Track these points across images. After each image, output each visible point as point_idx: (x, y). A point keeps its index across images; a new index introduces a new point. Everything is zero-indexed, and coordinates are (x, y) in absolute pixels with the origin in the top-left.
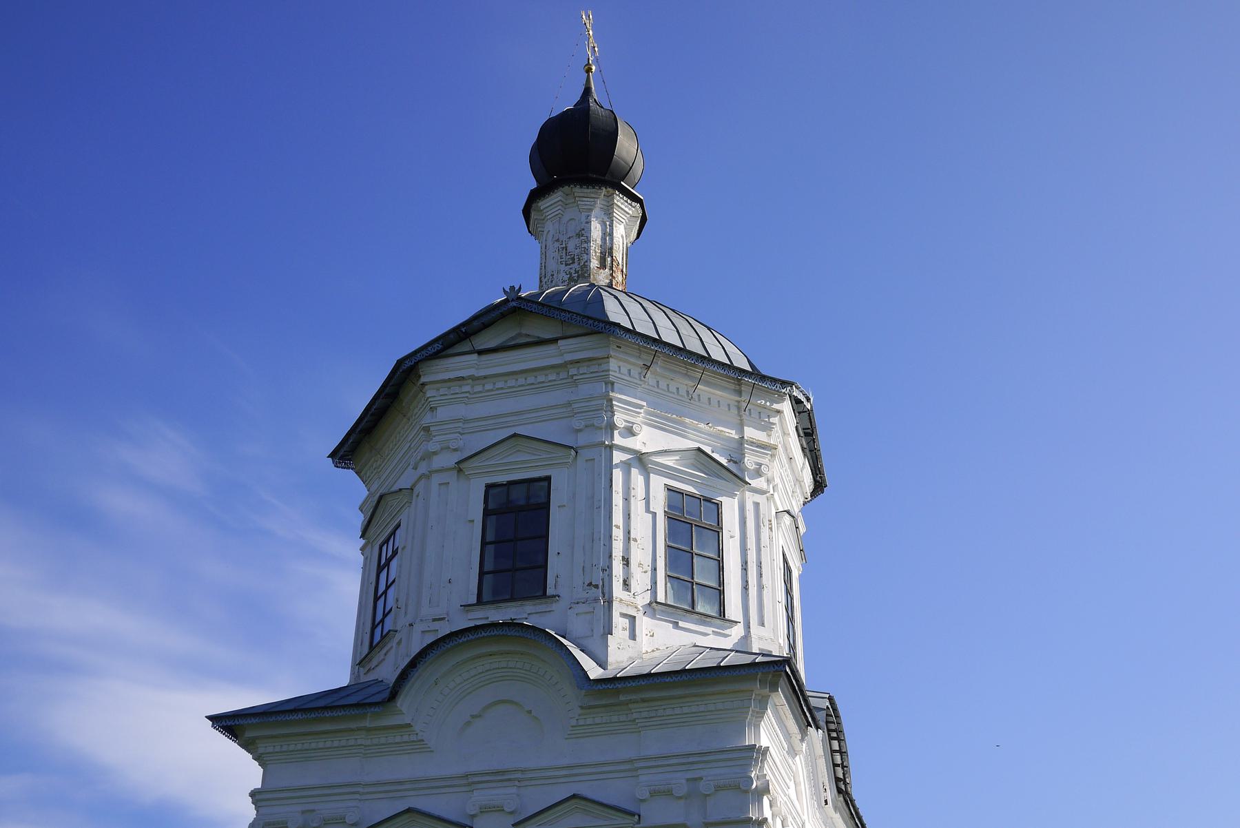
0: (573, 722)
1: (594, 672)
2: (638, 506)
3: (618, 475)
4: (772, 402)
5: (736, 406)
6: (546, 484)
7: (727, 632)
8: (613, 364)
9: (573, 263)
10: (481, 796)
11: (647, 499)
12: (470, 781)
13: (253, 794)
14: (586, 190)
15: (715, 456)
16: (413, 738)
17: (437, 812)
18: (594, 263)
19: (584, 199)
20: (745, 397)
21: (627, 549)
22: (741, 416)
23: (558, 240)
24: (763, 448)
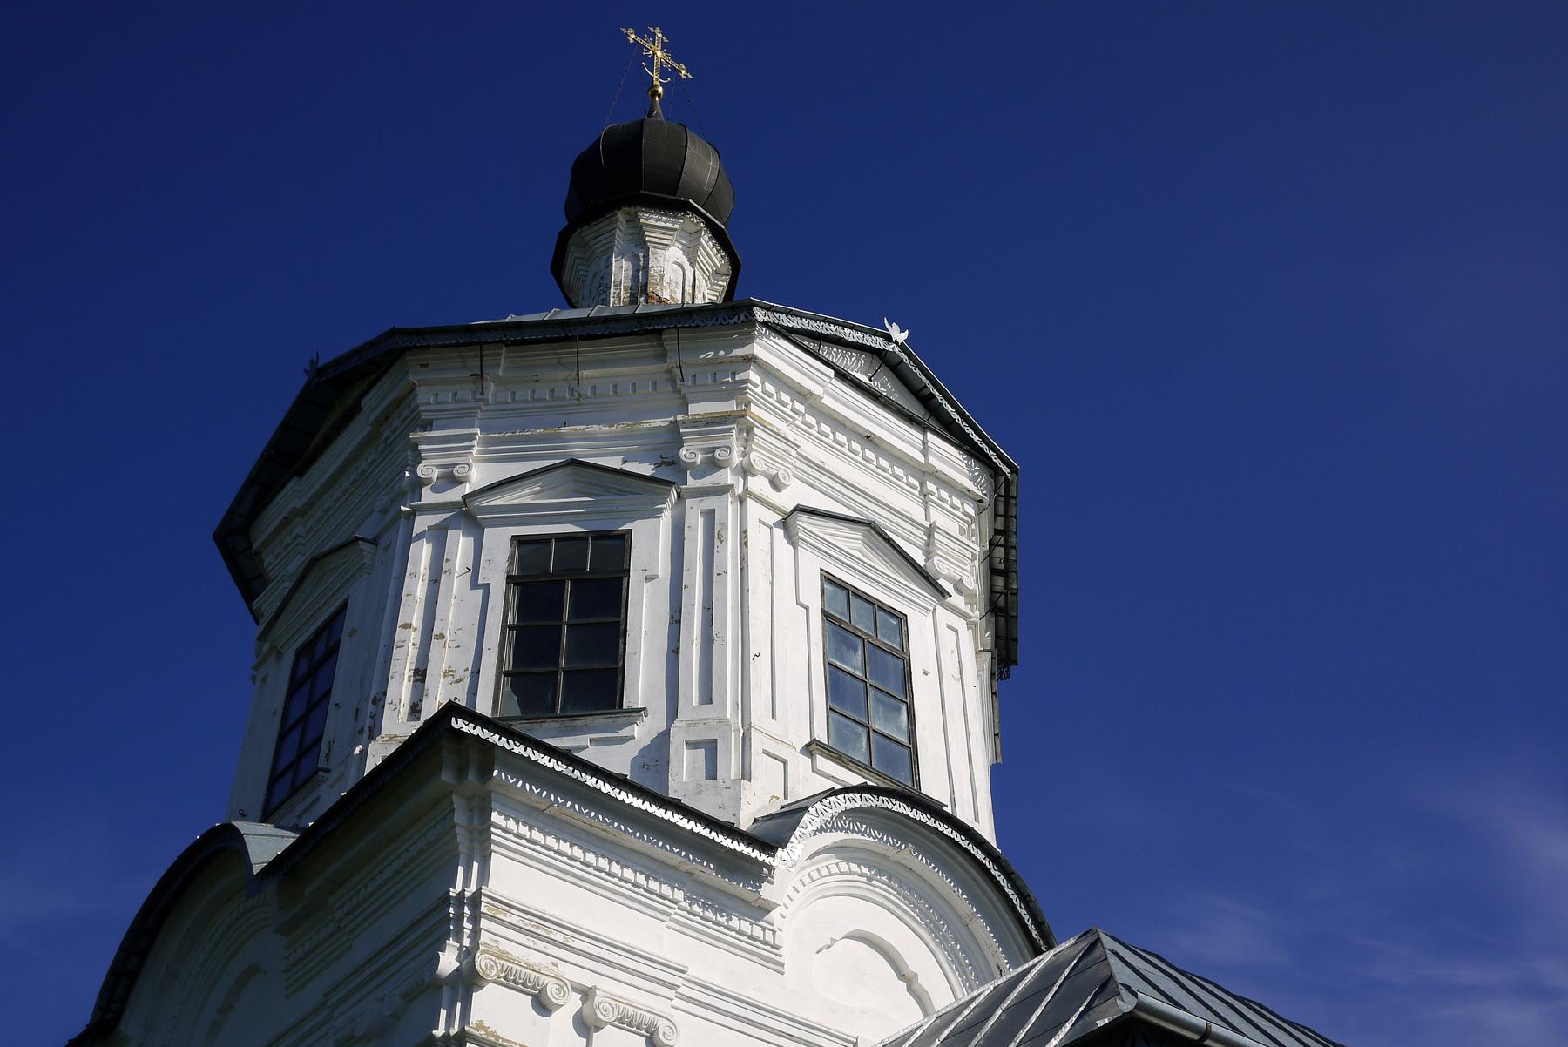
4: (729, 349)
5: (667, 380)
7: (624, 733)
15: (632, 467)
19: (600, 239)
20: (672, 360)
22: (679, 392)
24: (720, 423)
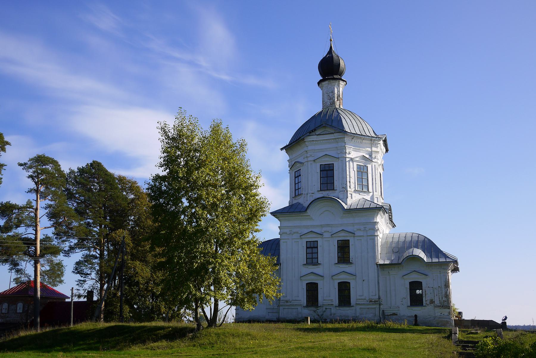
0: (341, 216)
1: (346, 207)
2: (351, 170)
3: (347, 163)
6: (333, 165)
7: (369, 194)
8: (346, 139)
9: (331, 99)
10: (324, 229)
11: (353, 168)
12: (322, 226)
13: (279, 227)
14: (333, 81)
16: (310, 217)
17: (316, 232)
18: (336, 100)
21: (350, 179)
23: (327, 93)
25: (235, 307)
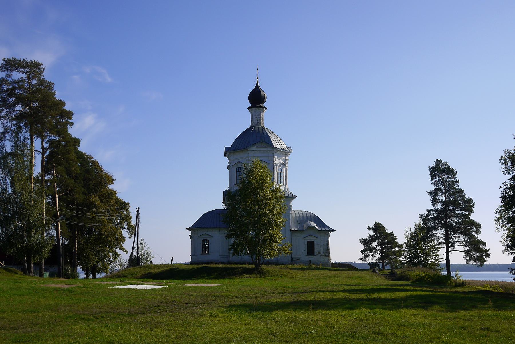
25: (470, 218)
